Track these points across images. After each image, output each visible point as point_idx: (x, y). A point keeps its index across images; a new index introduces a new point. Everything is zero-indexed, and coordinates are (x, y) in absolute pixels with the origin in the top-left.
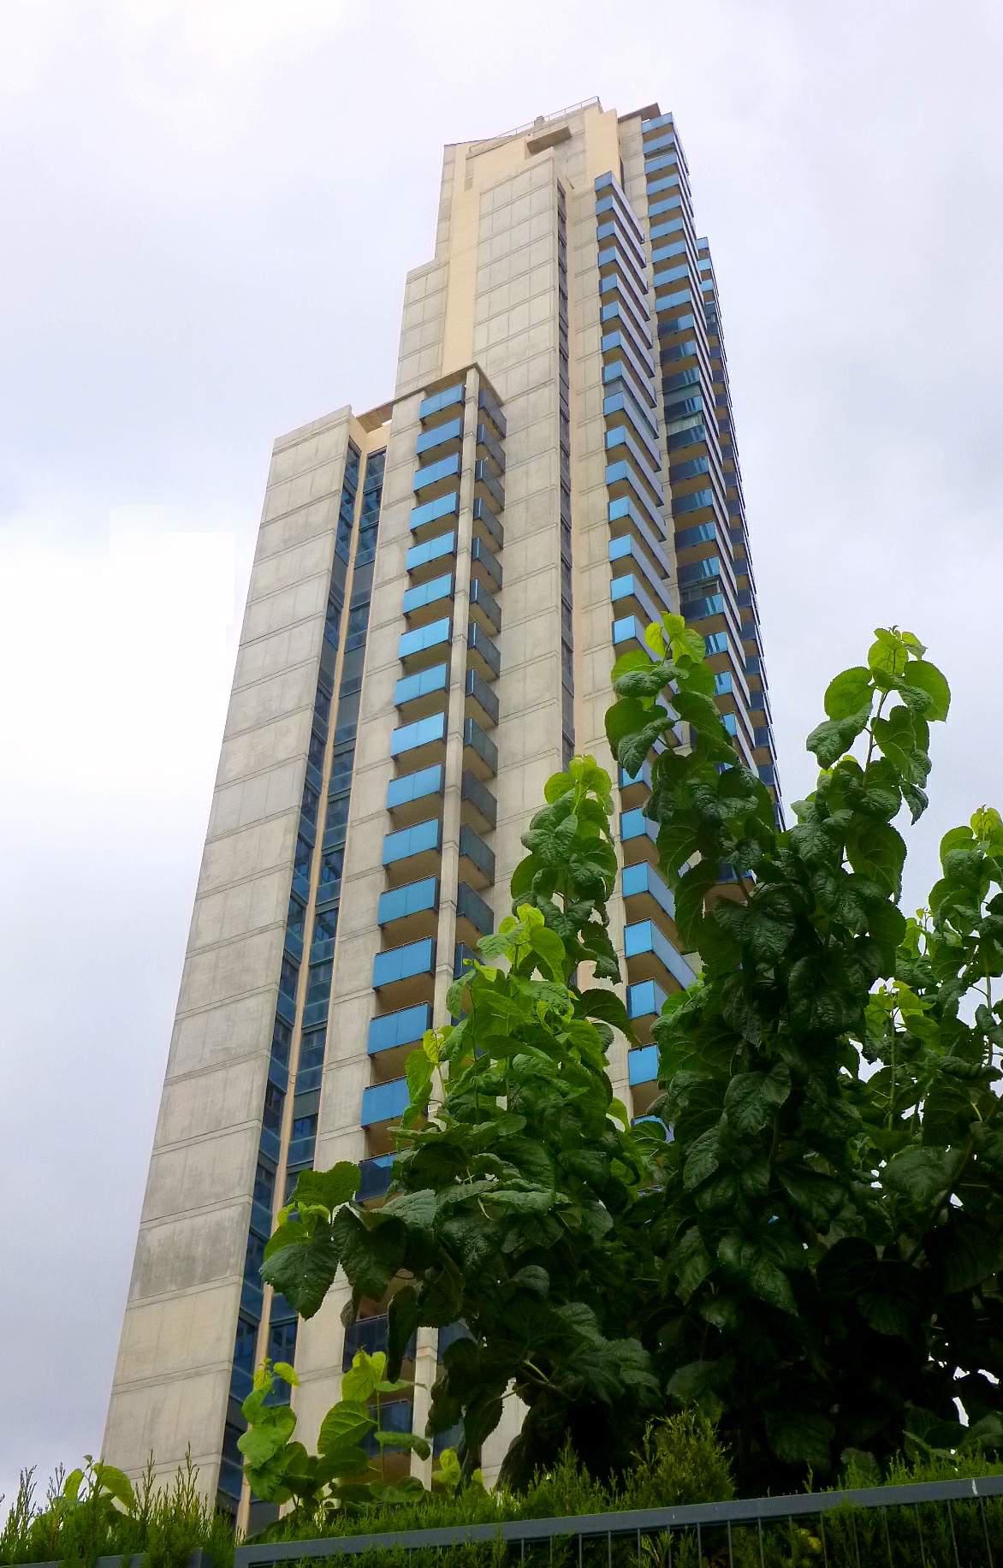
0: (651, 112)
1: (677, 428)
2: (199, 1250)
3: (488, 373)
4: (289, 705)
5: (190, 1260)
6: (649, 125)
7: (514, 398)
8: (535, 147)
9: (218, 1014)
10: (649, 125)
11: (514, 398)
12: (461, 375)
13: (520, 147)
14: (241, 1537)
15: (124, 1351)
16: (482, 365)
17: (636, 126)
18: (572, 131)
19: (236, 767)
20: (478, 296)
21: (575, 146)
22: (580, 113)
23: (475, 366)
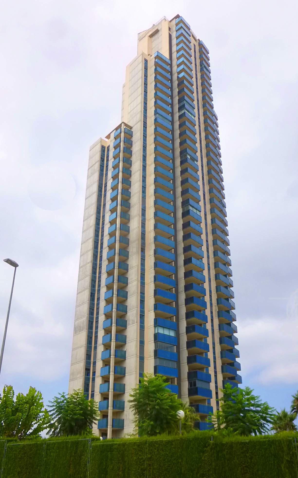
0: (178, 16)
1: (181, 113)
2: (81, 325)
3: (126, 122)
4: (92, 213)
5: (80, 327)
6: (178, 20)
7: (134, 125)
8: (151, 36)
9: (83, 280)
10: (178, 20)
11: (134, 125)
12: (120, 126)
13: (147, 38)
14: (176, 379)
15: (73, 343)
16: (124, 122)
17: (174, 22)
18: (159, 29)
19: (85, 228)
20: (129, 97)
21: (160, 33)
22: (160, 23)
23: (123, 122)
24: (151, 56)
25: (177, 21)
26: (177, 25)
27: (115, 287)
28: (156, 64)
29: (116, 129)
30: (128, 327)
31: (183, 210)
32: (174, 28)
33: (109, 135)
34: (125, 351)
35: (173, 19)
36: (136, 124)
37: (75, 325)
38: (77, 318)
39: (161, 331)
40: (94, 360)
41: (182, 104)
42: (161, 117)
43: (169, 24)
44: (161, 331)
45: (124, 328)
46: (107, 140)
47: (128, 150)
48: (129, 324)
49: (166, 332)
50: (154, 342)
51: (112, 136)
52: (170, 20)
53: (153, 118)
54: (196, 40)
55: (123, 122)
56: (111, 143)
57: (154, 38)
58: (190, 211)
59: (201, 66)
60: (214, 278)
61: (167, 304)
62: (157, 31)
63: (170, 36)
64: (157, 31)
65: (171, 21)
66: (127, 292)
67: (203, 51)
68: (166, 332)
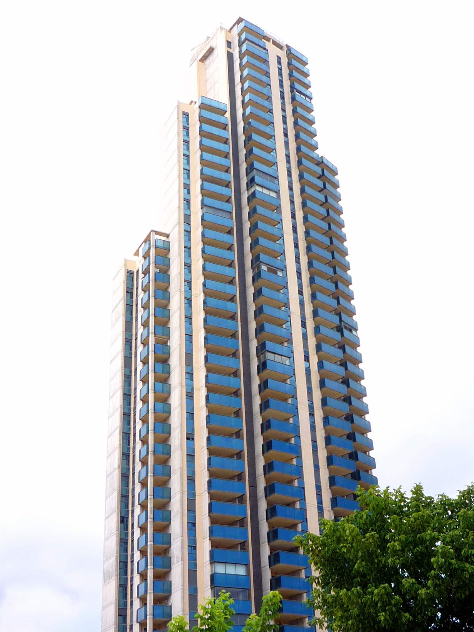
0: (240, 20)
4: (117, 388)
7: (171, 232)
8: (204, 59)
10: (242, 25)
11: (171, 232)
17: (236, 30)
21: (215, 52)
24: (195, 103)
25: (240, 29)
26: (240, 35)
27: (150, 506)
28: (202, 120)
29: (145, 241)
30: (173, 567)
31: (259, 360)
32: (235, 43)
33: (138, 250)
34: (171, 606)
35: (234, 26)
36: (173, 229)
37: (104, 570)
38: (106, 559)
39: (220, 569)
40: (130, 623)
41: (251, 176)
42: (210, 211)
43: (226, 35)
44: (220, 569)
45: (168, 570)
46: (136, 257)
47: (163, 273)
48: (174, 563)
49: (231, 570)
50: (211, 588)
51: (141, 253)
52: (228, 29)
53: (200, 213)
54: (281, 47)
55: (152, 231)
56: (138, 264)
57: (207, 62)
58: (268, 363)
59: (292, 92)
60: (326, 464)
61: (288, 505)
62: (211, 50)
63: (230, 56)
64: (211, 50)
65: (231, 29)
66: (170, 511)
67: (295, 65)
68: (231, 570)
